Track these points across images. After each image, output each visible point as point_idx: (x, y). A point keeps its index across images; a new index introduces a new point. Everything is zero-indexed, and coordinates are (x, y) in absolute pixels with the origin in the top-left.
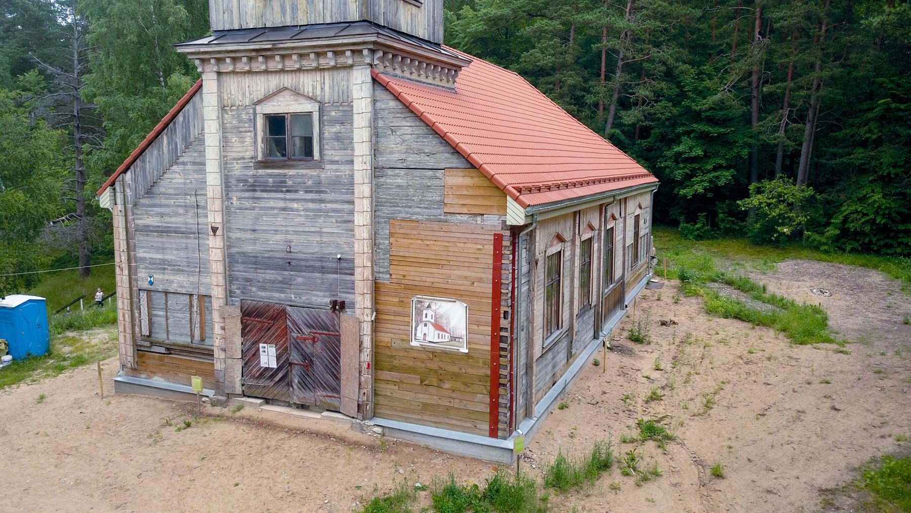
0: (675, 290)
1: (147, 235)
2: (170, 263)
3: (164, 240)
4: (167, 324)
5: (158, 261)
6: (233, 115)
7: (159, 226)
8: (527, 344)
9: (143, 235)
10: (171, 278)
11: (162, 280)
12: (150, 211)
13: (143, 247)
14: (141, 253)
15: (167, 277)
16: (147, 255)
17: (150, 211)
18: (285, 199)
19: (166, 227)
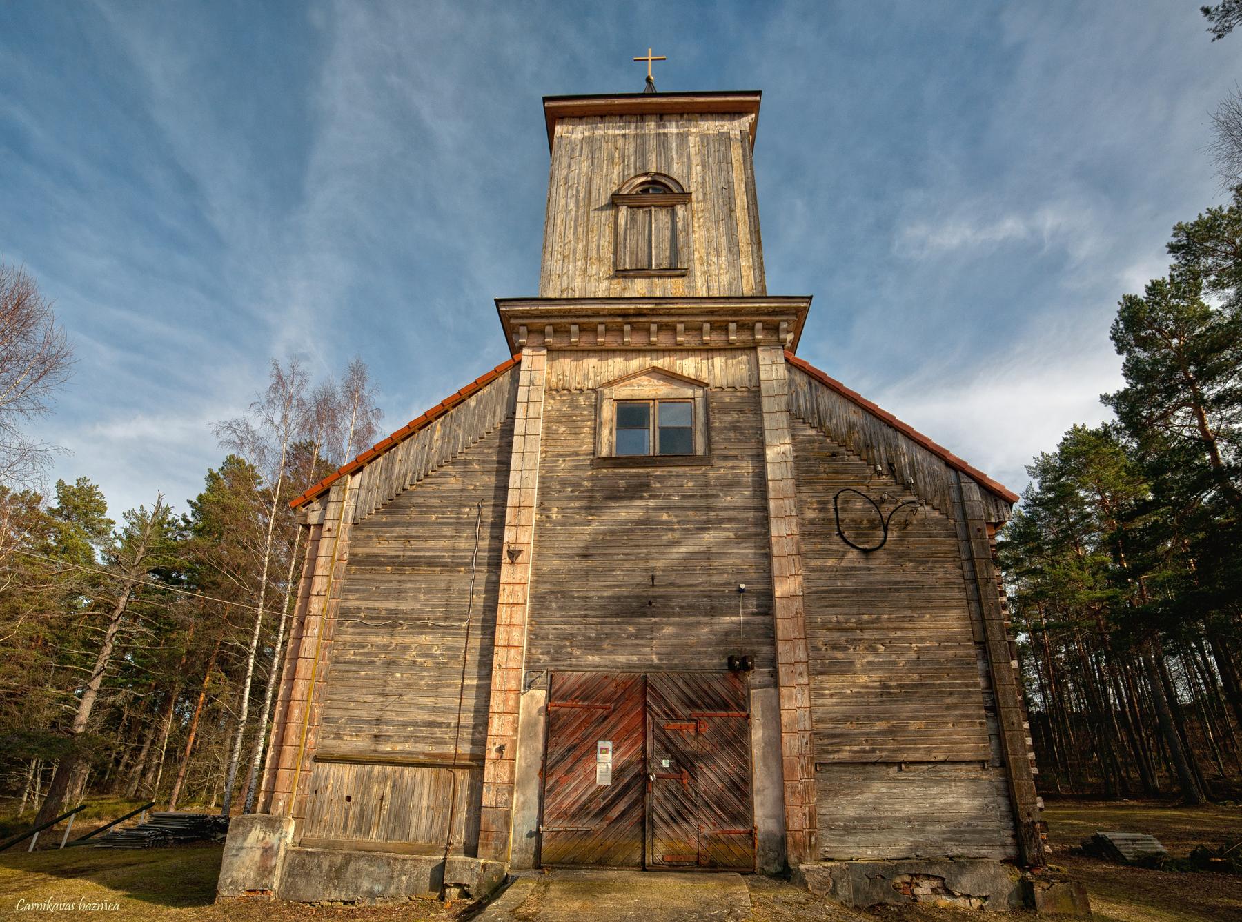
5: (384, 613)
7: (398, 557)
10: (407, 640)
12: (386, 533)
13: (357, 591)
16: (364, 604)
19: (411, 557)
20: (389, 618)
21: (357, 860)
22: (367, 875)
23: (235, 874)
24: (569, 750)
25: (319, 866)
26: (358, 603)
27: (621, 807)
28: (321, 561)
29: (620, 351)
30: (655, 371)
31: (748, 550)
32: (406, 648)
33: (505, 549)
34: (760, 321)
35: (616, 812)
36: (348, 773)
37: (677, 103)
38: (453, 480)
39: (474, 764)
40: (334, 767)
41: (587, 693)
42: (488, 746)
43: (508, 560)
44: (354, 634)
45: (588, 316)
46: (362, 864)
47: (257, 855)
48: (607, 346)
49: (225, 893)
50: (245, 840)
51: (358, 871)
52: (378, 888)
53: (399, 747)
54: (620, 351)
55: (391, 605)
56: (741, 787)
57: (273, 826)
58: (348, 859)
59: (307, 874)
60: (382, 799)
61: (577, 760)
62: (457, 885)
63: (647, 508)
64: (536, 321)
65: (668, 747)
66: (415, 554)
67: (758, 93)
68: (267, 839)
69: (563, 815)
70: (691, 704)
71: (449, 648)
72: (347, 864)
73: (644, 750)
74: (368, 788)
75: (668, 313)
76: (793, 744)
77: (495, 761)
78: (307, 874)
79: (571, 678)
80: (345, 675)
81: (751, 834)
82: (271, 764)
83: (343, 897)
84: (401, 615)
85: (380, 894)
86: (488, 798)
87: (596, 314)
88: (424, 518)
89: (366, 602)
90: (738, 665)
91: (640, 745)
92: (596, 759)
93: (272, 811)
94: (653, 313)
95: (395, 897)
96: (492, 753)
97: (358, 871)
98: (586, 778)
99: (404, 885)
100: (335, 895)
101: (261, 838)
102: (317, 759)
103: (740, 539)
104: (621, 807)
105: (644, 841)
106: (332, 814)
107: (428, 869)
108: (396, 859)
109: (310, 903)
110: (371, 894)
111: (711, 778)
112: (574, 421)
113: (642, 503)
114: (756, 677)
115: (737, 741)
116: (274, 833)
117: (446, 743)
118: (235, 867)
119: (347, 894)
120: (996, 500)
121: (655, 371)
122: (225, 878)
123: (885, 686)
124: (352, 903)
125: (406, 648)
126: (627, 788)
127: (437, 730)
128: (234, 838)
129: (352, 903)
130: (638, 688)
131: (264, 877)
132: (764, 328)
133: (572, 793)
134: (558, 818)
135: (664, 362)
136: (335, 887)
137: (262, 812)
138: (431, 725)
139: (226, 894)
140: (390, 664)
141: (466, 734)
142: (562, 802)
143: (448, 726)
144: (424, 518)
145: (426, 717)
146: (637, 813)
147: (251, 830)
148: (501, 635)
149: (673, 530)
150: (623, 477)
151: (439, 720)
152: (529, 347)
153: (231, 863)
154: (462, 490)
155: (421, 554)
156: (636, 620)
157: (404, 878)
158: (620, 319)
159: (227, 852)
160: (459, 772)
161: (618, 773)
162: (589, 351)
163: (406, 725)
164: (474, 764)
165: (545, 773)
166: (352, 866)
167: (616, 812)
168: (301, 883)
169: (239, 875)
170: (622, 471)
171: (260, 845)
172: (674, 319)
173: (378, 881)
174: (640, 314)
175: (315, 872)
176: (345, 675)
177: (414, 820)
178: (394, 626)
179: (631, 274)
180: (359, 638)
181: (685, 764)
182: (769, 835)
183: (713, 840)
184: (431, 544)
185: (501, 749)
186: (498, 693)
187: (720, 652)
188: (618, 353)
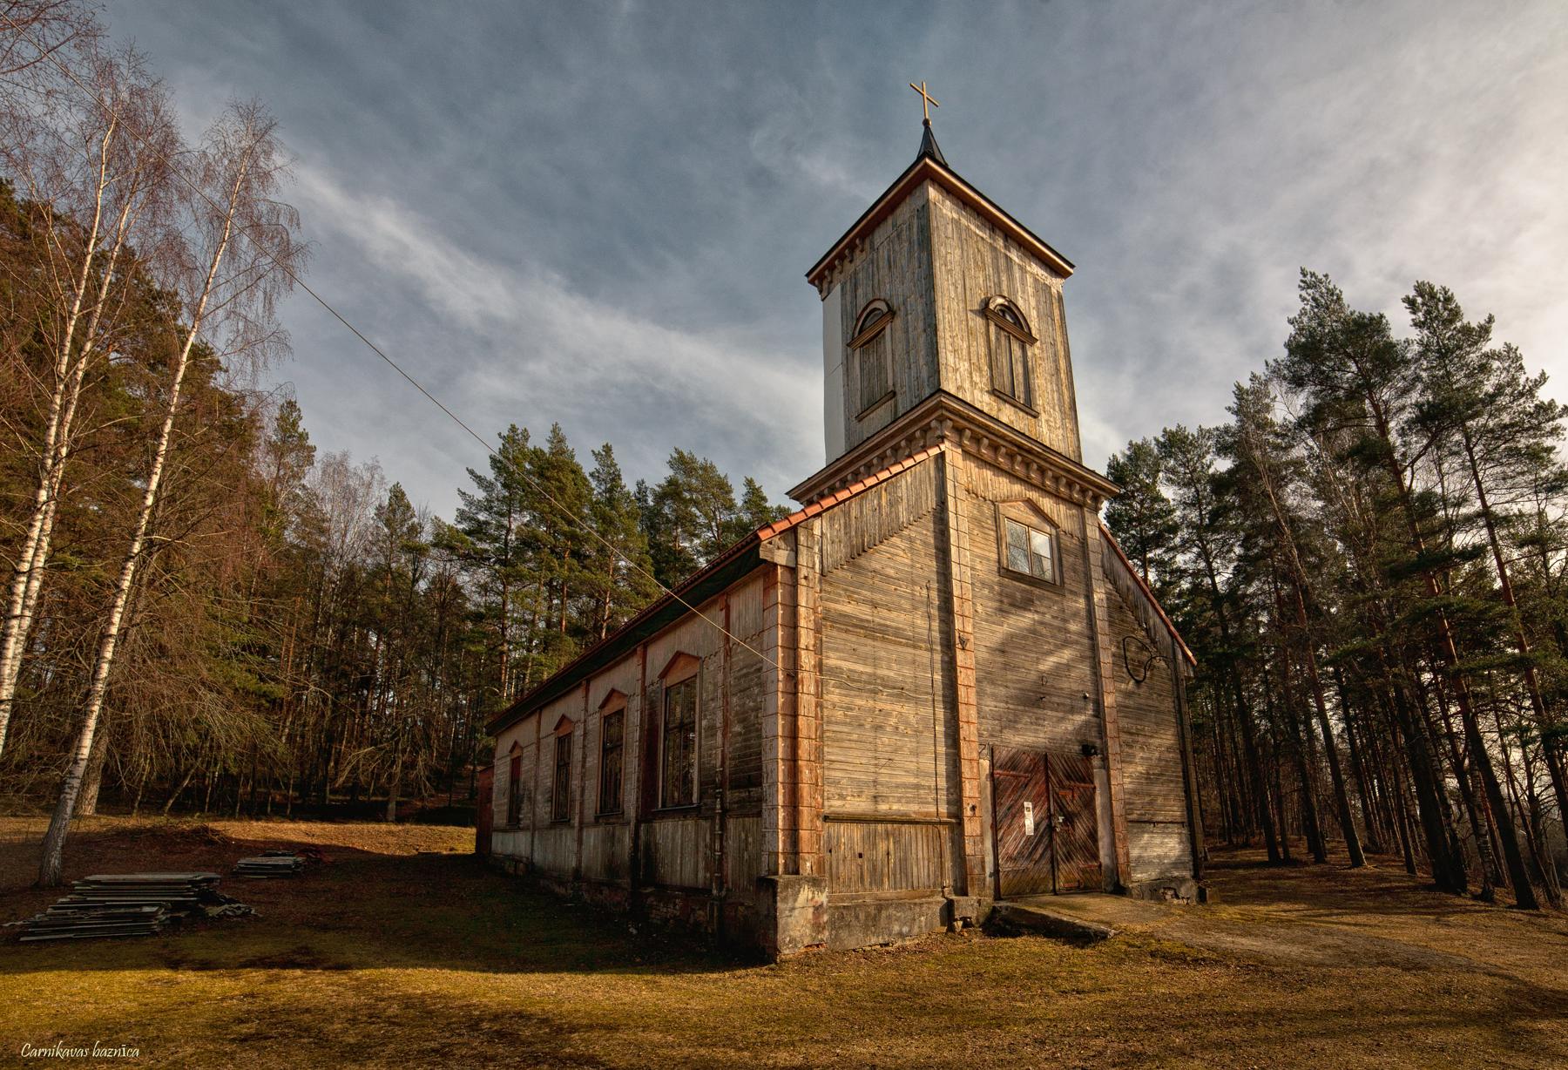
0: (676, 455)
1: (847, 631)
2: (886, 683)
3: (875, 643)
4: (935, 746)
5: (864, 677)
6: (1314, 589)
7: (868, 621)
8: (969, 422)
9: (839, 630)
10: (888, 707)
11: (872, 710)
12: (854, 592)
13: (837, 650)
14: (832, 661)
15: (880, 705)
16: (845, 665)
17: (854, 592)
18: (583, 777)
19: (880, 625)
20: (870, 683)
21: (887, 908)
22: (896, 920)
23: (792, 933)
24: (1009, 809)
25: (857, 917)
26: (839, 663)
27: (1040, 851)
28: (802, 611)
29: (1009, 473)
30: (1030, 503)
31: (1084, 669)
32: (888, 714)
33: (957, 635)
34: (951, 420)
35: (1037, 856)
36: (856, 832)
37: (1022, 236)
38: (902, 553)
39: (953, 820)
40: (843, 827)
41: (1012, 764)
42: (965, 805)
43: (960, 646)
44: (840, 694)
45: (996, 436)
46: (891, 911)
47: (810, 913)
48: (1002, 466)
49: (786, 952)
50: (795, 900)
51: (889, 917)
52: (905, 929)
53: (895, 807)
54: (1009, 473)
55: (869, 670)
56: (1093, 835)
57: (819, 886)
58: (880, 908)
59: (848, 925)
60: (888, 854)
61: (1014, 816)
62: (961, 919)
63: (1034, 619)
64: (961, 421)
65: (1062, 809)
66: (882, 622)
67: (1072, 266)
68: (816, 898)
69: (1010, 858)
70: (1068, 777)
71: (923, 719)
72: (880, 911)
73: (1049, 809)
74: (875, 845)
75: (1045, 460)
76: (1117, 807)
77: (970, 818)
78: (848, 925)
79: (1003, 754)
80: (839, 736)
81: (1100, 866)
82: (784, 825)
83: (881, 941)
84: (879, 681)
85: (909, 934)
86: (969, 849)
87: (1003, 437)
88: (885, 586)
89: (847, 663)
90: (1087, 750)
91: (1046, 806)
92: (1024, 816)
93: (801, 871)
94: (1038, 455)
95: (918, 935)
96: (968, 812)
97: (889, 917)
98: (1020, 831)
99: (923, 924)
100: (874, 940)
101: (810, 896)
102: (826, 818)
103: (1082, 658)
104: (1040, 851)
105: (1054, 875)
106: (847, 870)
107: (937, 909)
108: (915, 904)
109: (854, 950)
110: (901, 935)
111: (1080, 830)
112: (983, 527)
113: (1029, 615)
114: (1096, 761)
115: (1089, 804)
116: (822, 893)
117: (929, 803)
118: (791, 927)
119: (883, 938)
120: (610, 502)
121: (1030, 503)
122: (783, 937)
123: (1148, 774)
124: (887, 945)
125: (888, 714)
126: (1042, 836)
127: (922, 792)
128: (785, 900)
129: (887, 945)
130: (1042, 763)
131: (819, 932)
132: (1007, 454)
133: (1010, 845)
134: (1007, 861)
135: (1033, 495)
136: (873, 934)
137: (786, 872)
138: (917, 787)
139: (787, 952)
140: (878, 728)
141: (943, 796)
142: (1008, 849)
143: (929, 787)
144: (885, 586)
145: (913, 780)
146: (1048, 854)
147: (799, 891)
148: (962, 709)
149: (1049, 643)
150: (1018, 589)
151: (923, 783)
152: (949, 441)
153: (787, 924)
154: (912, 567)
155: (888, 623)
156: (1035, 710)
157: (922, 918)
158: (1016, 449)
159: (781, 914)
160: (941, 828)
161: (1037, 826)
162: (990, 464)
163: (897, 786)
164: (953, 820)
165: (995, 827)
166: (884, 914)
167: (1037, 856)
168: (844, 934)
169: (796, 934)
170: (1017, 584)
171: (811, 904)
172: (1048, 465)
173: (905, 924)
174: (1030, 451)
175: (854, 922)
176: (839, 736)
177: (915, 869)
178: (875, 692)
179: (1005, 397)
180: (847, 700)
181: (1070, 819)
182: (1107, 867)
183: (1083, 871)
184: (894, 615)
185: (973, 808)
186: (966, 762)
187: (1079, 741)
188: (972, 458)
